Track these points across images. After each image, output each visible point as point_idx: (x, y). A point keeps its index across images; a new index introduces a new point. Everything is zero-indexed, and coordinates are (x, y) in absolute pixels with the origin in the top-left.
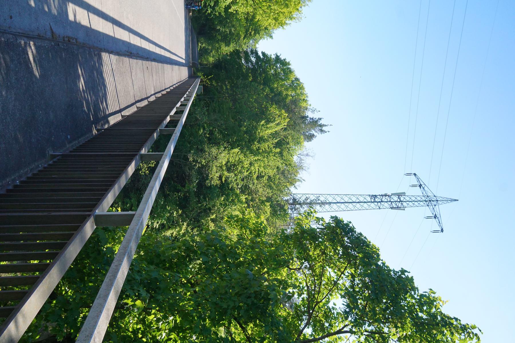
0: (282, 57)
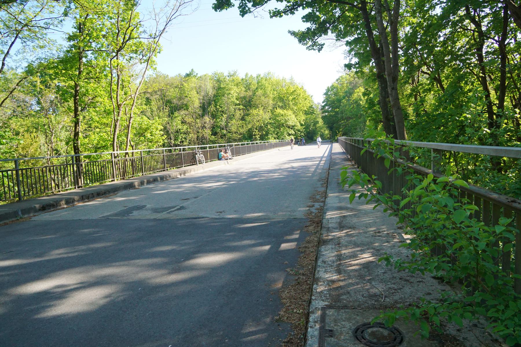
0: (325, 91)
